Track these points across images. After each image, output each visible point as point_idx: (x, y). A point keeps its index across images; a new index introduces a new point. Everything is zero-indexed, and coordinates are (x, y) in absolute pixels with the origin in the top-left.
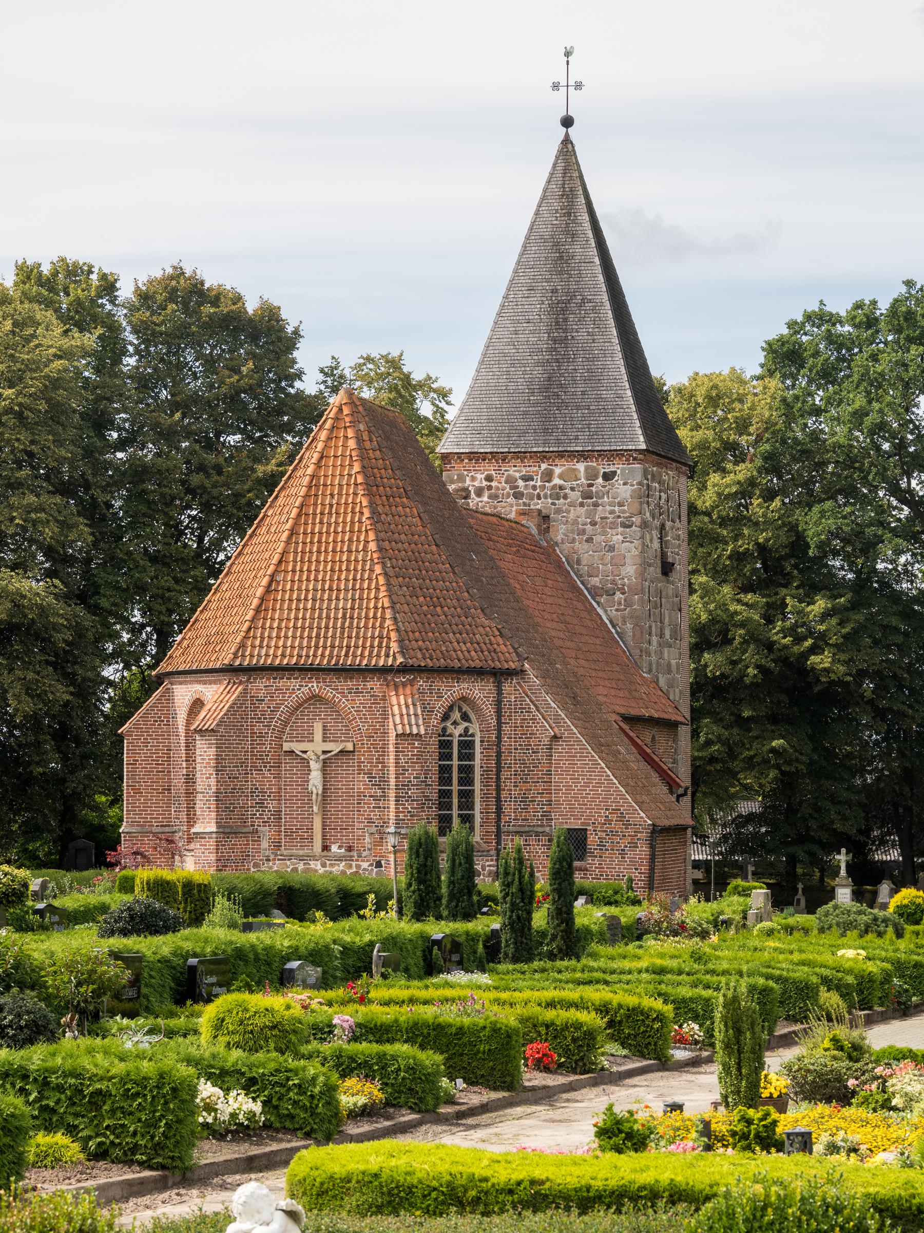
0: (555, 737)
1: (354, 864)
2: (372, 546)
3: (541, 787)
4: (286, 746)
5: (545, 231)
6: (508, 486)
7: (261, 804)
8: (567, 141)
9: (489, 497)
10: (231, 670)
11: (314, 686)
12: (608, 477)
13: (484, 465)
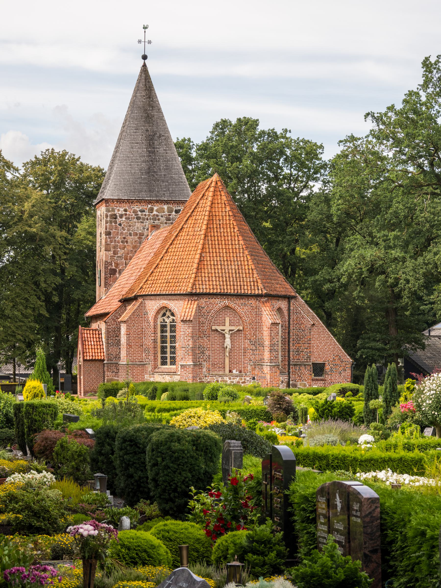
0: (314, 324)
2: (241, 242)
4: (213, 328)
5: (140, 104)
6: (134, 214)
7: (203, 352)
8: (144, 65)
9: (126, 219)
11: (226, 302)
13: (124, 204)
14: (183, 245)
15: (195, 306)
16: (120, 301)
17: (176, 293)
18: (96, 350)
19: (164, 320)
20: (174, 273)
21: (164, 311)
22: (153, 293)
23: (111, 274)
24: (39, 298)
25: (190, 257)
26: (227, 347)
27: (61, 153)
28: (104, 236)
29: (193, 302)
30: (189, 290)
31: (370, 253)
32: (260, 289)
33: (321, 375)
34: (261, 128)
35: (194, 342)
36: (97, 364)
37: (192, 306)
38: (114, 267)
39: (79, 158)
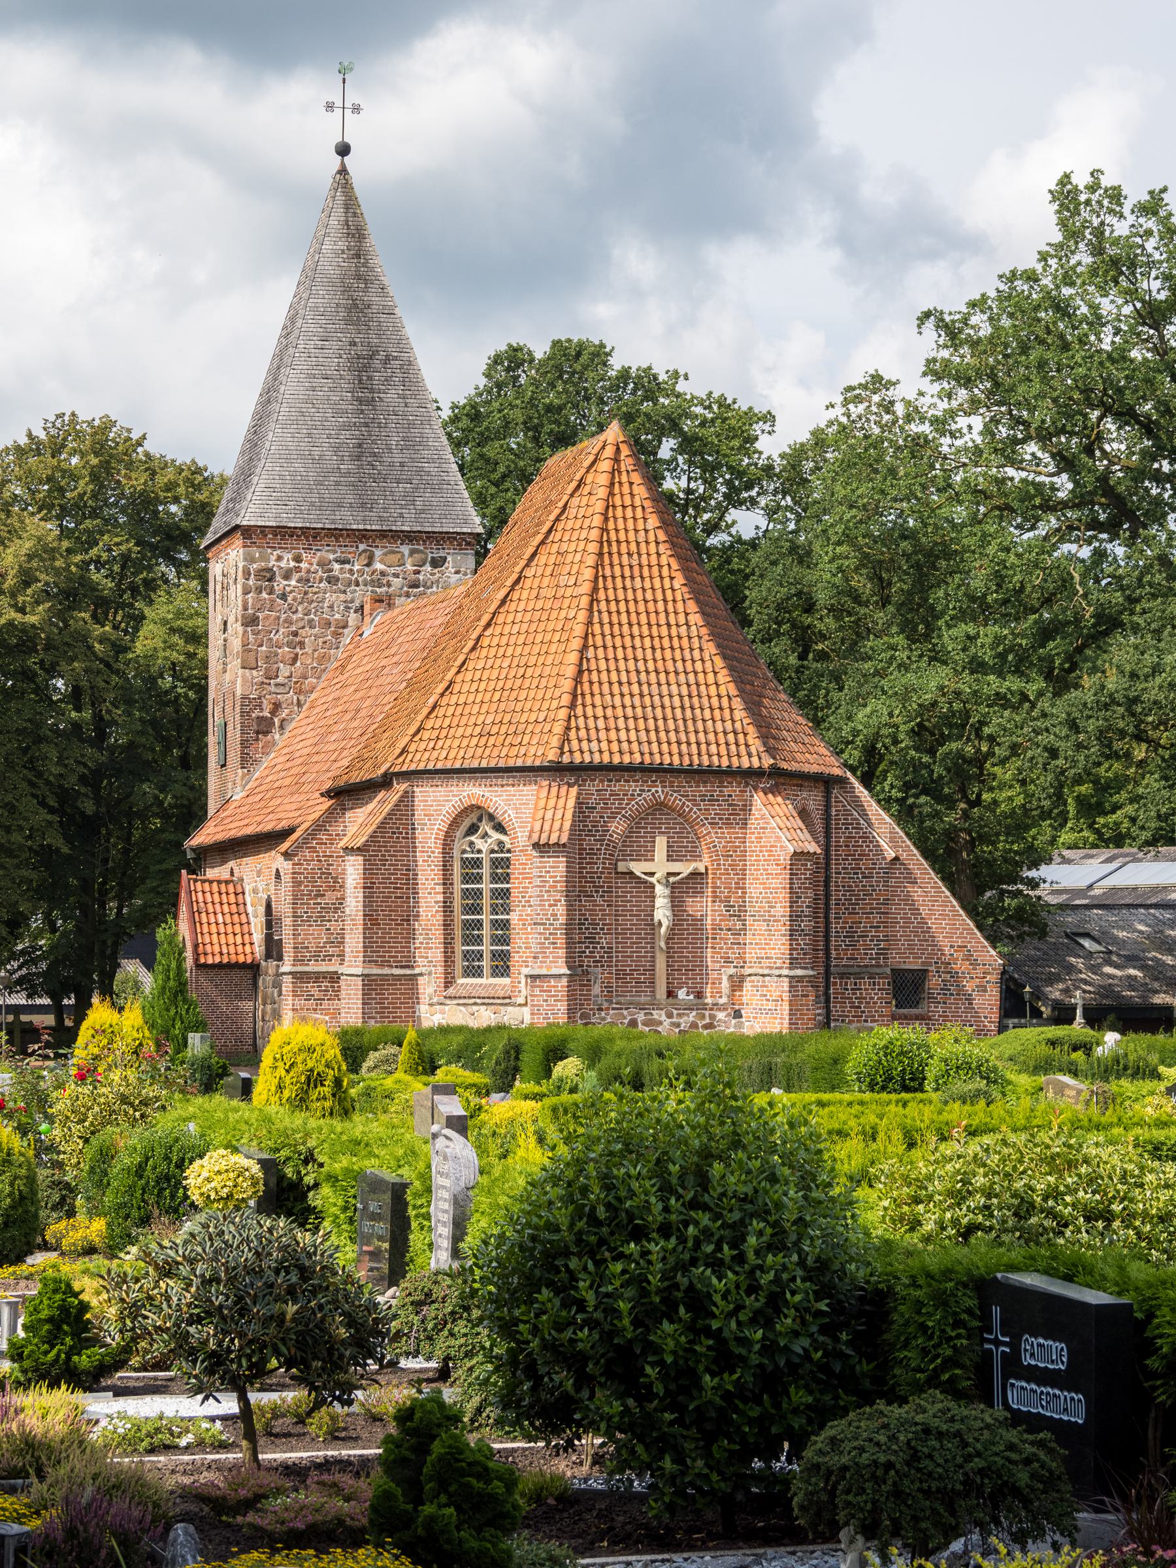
1: (707, 1013)
3: (876, 919)
4: (622, 867)
7: (592, 939)
8: (343, 171)
10: (558, 770)
12: (437, 563)
14: (525, 626)
15: (571, 803)
16: (329, 794)
17: (511, 763)
18: (231, 936)
19: (471, 844)
20: (502, 706)
21: (474, 818)
22: (439, 766)
23: (258, 733)
24: (43, 803)
25: (549, 662)
26: (660, 924)
27: (97, 423)
28: (236, 628)
29: (564, 789)
30: (552, 755)
31: (932, 682)
32: (755, 756)
33: (916, 1004)
34: (617, 363)
35: (570, 908)
36: (236, 975)
37: (561, 802)
38: (267, 714)
39: (144, 437)
